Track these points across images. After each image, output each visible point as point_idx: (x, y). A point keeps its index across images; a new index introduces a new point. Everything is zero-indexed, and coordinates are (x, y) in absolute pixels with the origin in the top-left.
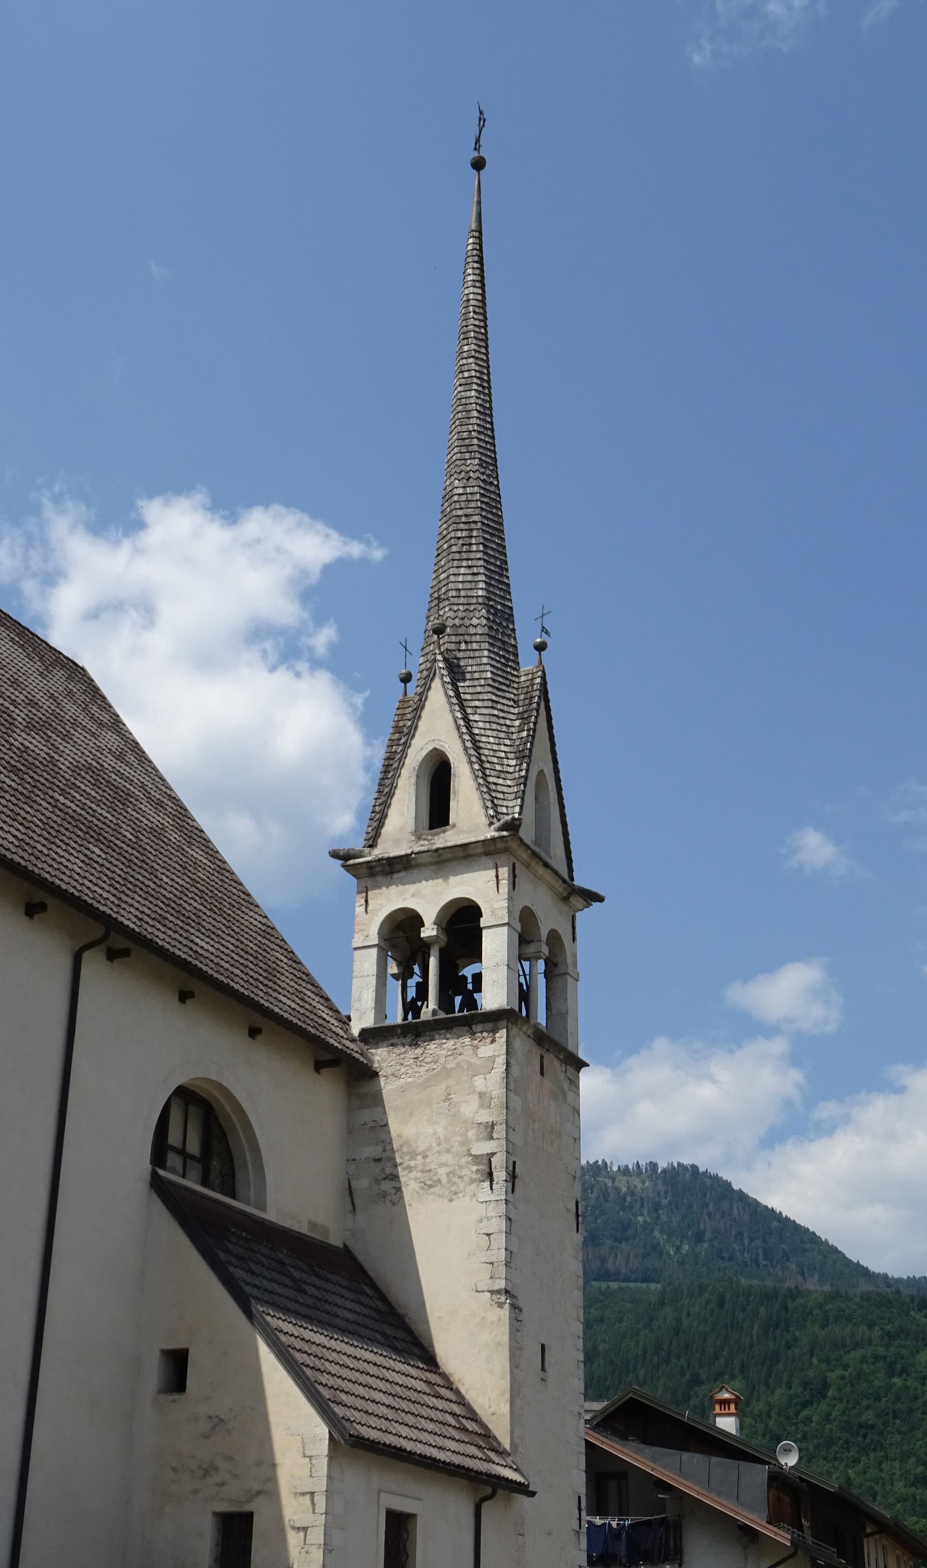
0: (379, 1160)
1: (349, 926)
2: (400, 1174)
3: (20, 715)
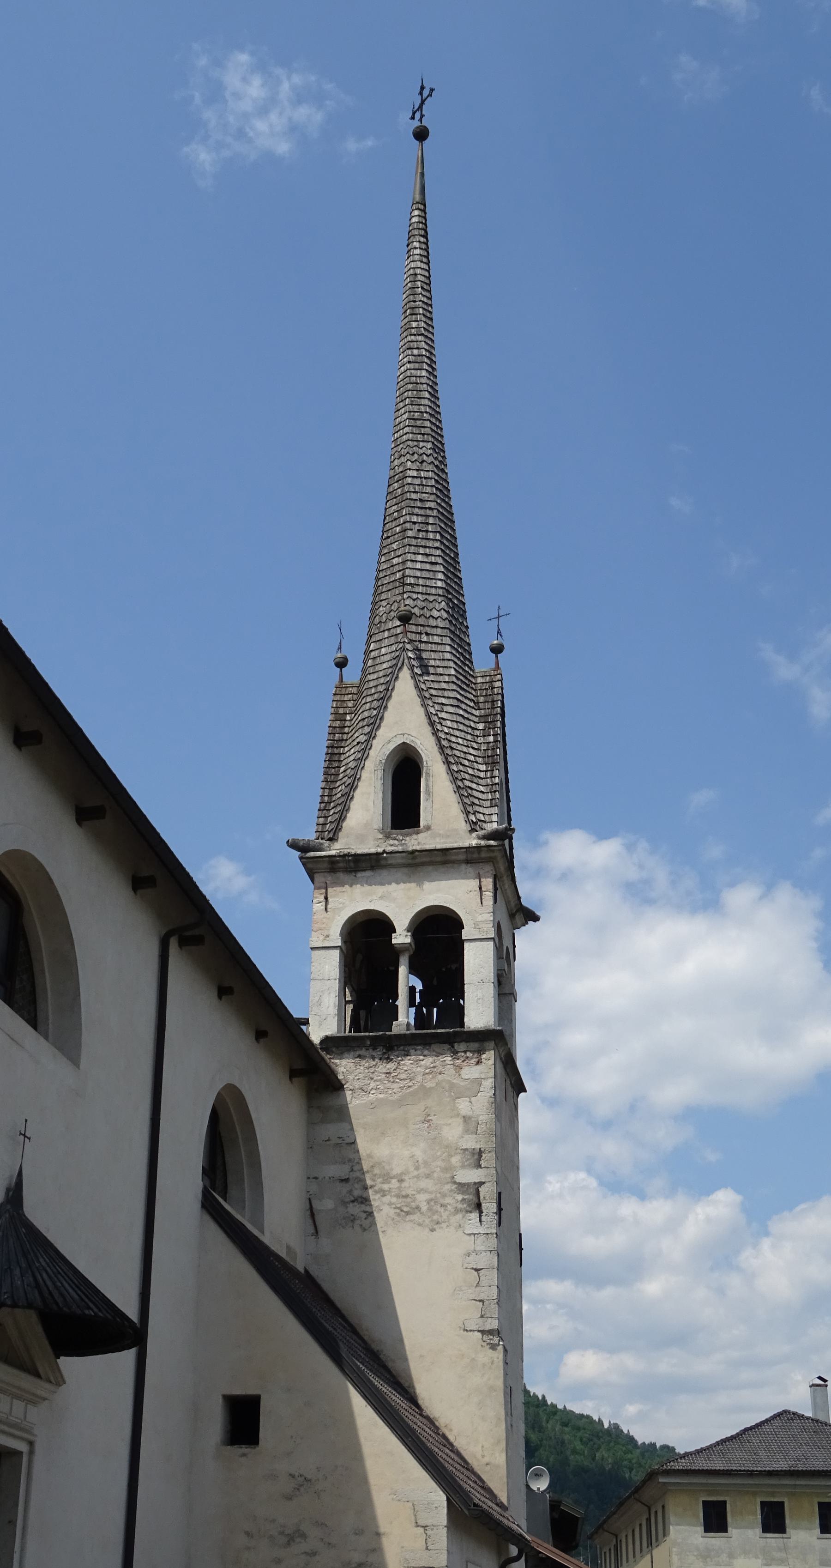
0: (346, 1180)
2: (372, 1197)
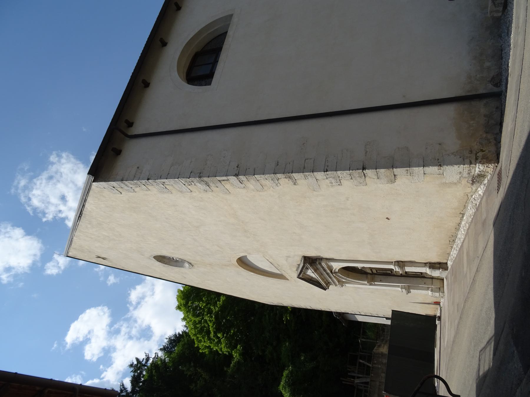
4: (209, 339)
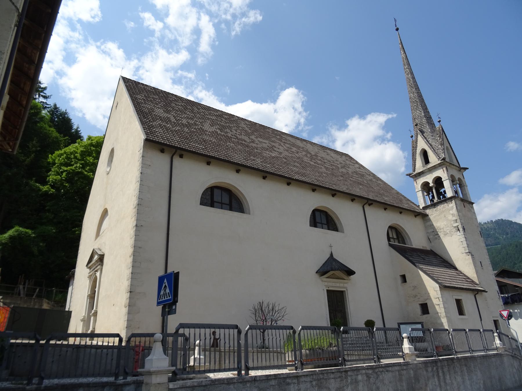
1: (414, 188)
3: (339, 166)
4: (61, 164)
